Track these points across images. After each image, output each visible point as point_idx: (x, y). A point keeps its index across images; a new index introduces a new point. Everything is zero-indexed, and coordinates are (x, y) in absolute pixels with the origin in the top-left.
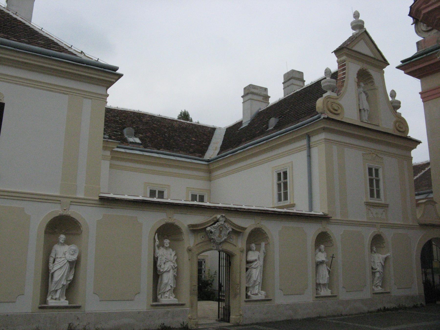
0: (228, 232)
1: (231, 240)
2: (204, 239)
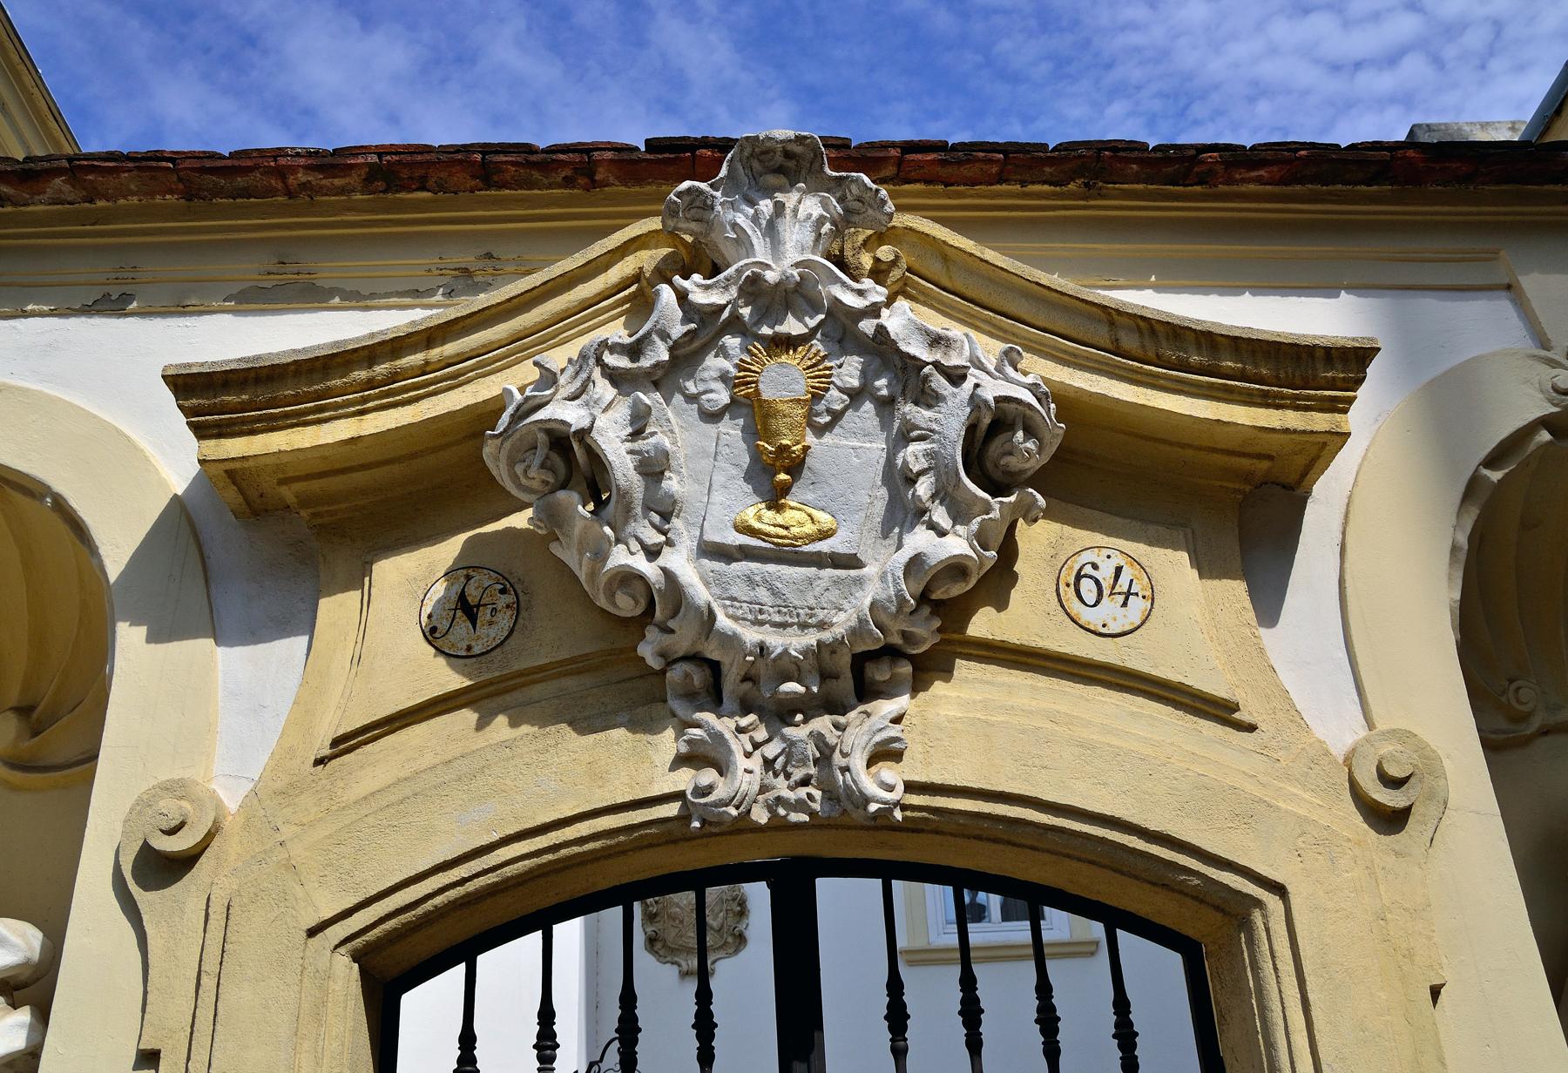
0: (948, 420)
1: (1110, 614)
2: (490, 632)
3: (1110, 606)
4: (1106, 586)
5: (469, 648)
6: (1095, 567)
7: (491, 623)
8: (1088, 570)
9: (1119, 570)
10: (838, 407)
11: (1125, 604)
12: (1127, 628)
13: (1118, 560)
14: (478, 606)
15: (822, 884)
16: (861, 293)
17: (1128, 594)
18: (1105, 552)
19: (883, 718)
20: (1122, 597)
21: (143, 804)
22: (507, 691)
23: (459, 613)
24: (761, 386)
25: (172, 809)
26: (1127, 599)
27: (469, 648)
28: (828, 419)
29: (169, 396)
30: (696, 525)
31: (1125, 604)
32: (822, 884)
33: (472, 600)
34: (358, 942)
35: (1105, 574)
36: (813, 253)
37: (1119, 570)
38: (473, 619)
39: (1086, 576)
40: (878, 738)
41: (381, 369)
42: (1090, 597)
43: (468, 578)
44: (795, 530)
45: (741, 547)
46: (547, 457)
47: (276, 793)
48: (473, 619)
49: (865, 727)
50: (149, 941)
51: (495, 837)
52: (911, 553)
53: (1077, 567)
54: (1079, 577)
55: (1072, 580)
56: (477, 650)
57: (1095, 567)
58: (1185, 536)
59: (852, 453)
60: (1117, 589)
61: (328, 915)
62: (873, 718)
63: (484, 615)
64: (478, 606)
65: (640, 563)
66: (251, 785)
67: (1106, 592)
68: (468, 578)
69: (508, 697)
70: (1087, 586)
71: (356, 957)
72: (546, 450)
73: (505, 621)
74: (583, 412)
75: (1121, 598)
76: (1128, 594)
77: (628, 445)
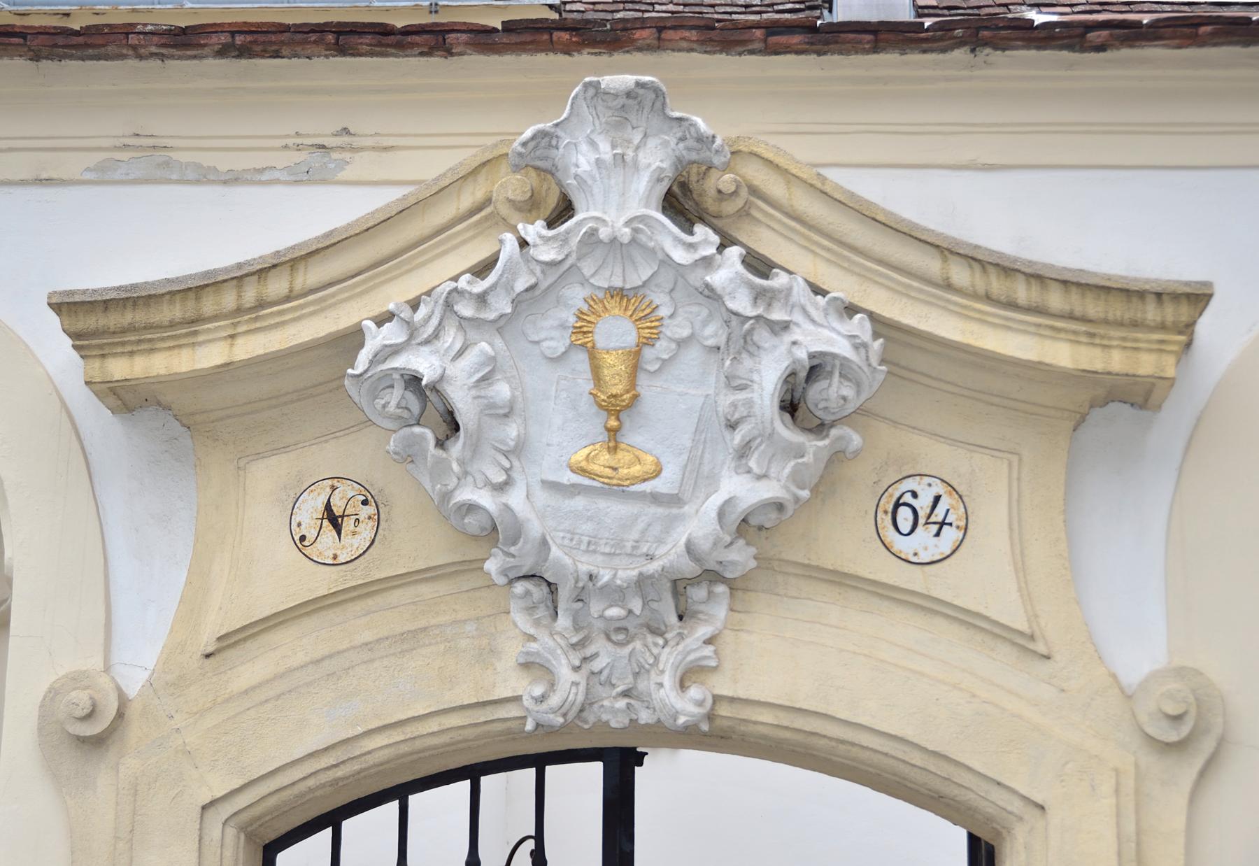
1: (923, 543)
3: (924, 534)
4: (922, 514)
5: (335, 557)
6: (915, 495)
7: (354, 533)
8: (908, 498)
9: (937, 499)
10: (665, 356)
11: (938, 534)
12: (935, 558)
13: (938, 488)
14: (343, 516)
15: (533, 770)
16: (691, 247)
17: (942, 524)
18: (927, 480)
19: (697, 639)
20: (936, 527)
21: (53, 693)
22: (368, 595)
23: (326, 522)
24: (596, 337)
25: (82, 698)
26: (940, 529)
27: (335, 557)
28: (657, 367)
29: (53, 319)
30: (541, 465)
31: (938, 534)
32: (533, 770)
33: (337, 511)
34: (244, 817)
35: (923, 504)
36: (647, 206)
37: (937, 499)
38: (337, 528)
39: (906, 504)
40: (691, 657)
41: (250, 294)
42: (905, 526)
43: (334, 488)
44: (623, 472)
45: (573, 485)
46: (403, 397)
47: (169, 681)
48: (337, 528)
49: (680, 647)
50: (818, 731)
51: (360, 730)
52: (726, 497)
53: (897, 495)
54: (897, 505)
55: (890, 508)
56: (341, 559)
57: (915, 495)
58: (1010, 465)
59: (679, 398)
60: (933, 519)
61: (219, 794)
62: (688, 641)
63: (348, 525)
64: (343, 516)
65: (485, 499)
66: (146, 675)
67: (922, 521)
68: (334, 488)
69: (370, 602)
70: (905, 515)
71: (242, 828)
72: (401, 391)
73: (366, 531)
74: (436, 361)
75: (935, 528)
76: (942, 524)
77: (473, 392)
